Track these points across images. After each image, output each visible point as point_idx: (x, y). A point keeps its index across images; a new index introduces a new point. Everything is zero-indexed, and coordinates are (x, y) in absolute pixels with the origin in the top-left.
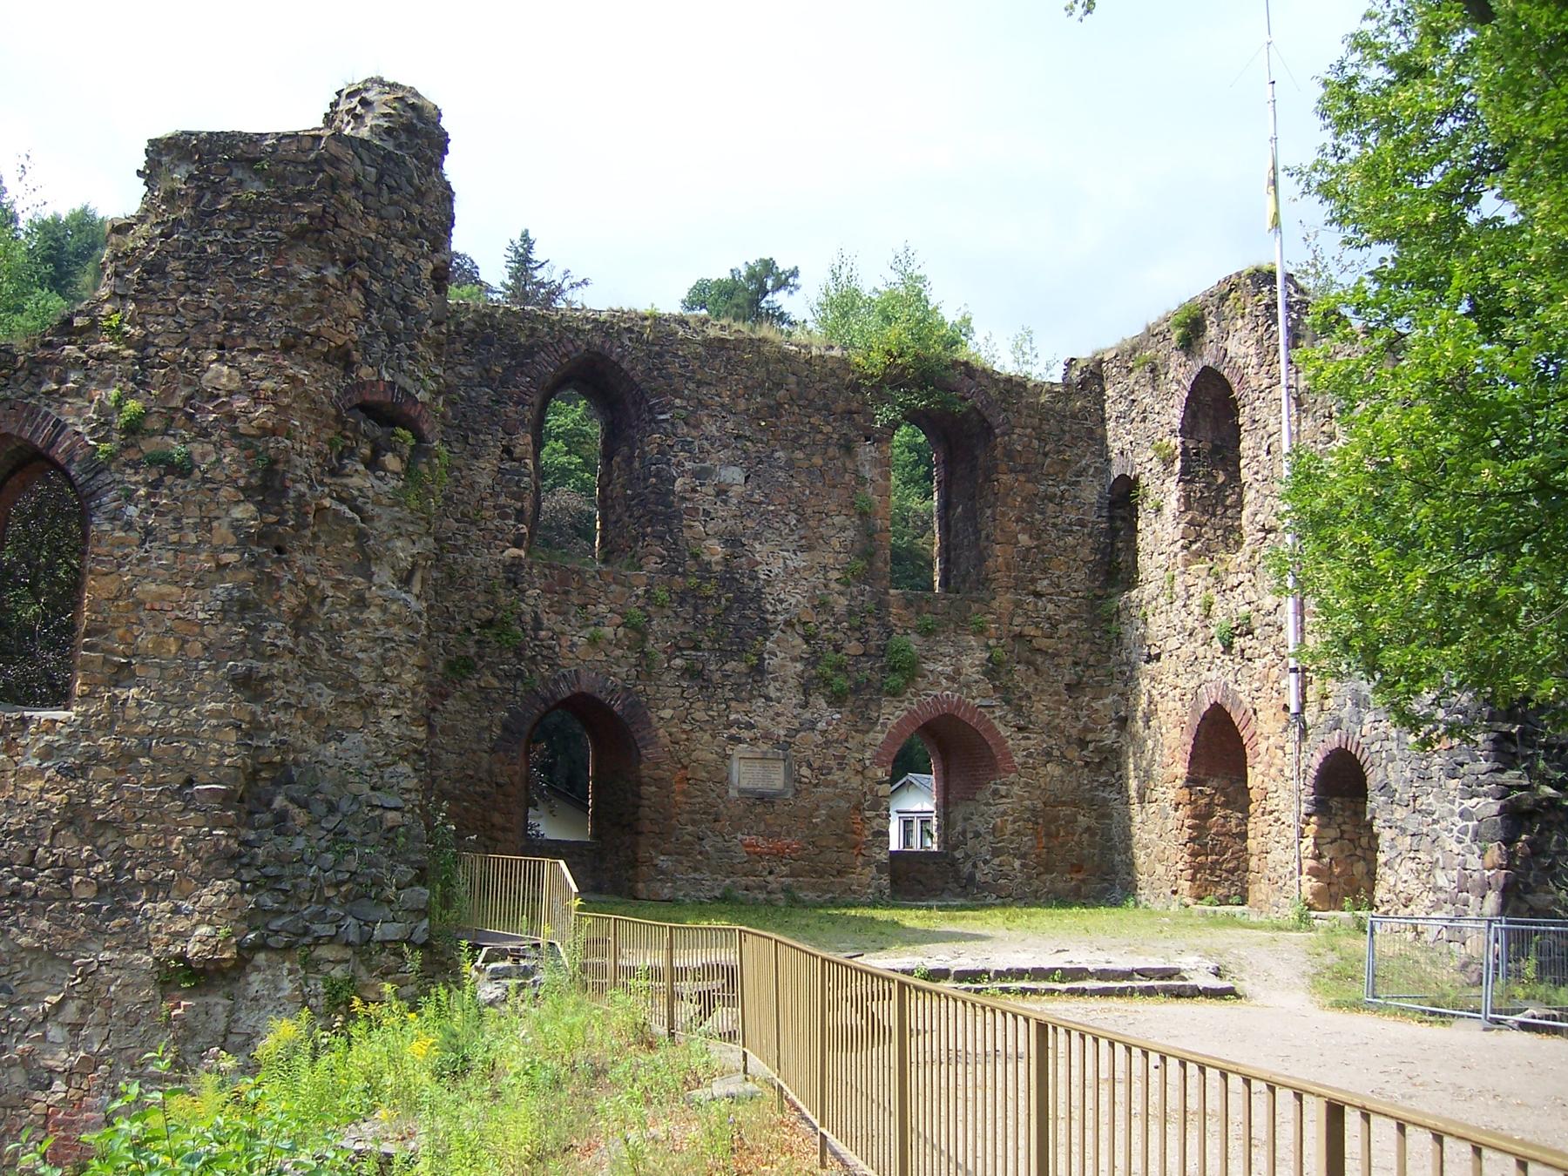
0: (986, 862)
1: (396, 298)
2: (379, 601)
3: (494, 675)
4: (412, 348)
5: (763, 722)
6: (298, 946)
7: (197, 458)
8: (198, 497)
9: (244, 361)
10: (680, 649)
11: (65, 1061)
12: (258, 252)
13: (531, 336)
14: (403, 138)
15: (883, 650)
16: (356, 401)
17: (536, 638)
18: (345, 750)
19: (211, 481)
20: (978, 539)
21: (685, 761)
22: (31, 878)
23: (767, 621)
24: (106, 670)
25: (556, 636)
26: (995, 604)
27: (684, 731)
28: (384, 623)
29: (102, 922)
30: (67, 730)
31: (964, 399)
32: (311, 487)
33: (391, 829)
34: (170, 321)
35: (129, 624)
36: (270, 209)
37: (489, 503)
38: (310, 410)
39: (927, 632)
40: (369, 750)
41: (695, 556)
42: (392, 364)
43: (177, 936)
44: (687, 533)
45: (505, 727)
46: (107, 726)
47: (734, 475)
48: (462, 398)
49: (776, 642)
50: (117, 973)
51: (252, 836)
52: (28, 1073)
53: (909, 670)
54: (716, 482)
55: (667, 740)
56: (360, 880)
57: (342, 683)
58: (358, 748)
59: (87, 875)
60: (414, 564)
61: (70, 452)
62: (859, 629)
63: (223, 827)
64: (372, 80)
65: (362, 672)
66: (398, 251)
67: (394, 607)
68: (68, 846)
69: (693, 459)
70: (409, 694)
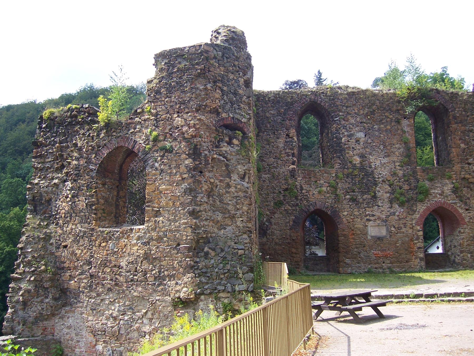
0: (458, 255)
1: (232, 91)
2: (234, 185)
3: (289, 205)
4: (239, 106)
5: (377, 214)
6: (214, 293)
7: (174, 147)
8: (175, 159)
9: (185, 116)
10: (348, 192)
11: (148, 329)
12: (186, 82)
13: (292, 98)
14: (231, 42)
15: (416, 187)
16: (221, 124)
17: (302, 193)
18: (226, 232)
19: (178, 153)
20: (447, 147)
21: (353, 228)
22: (136, 276)
23: (376, 181)
24: (153, 213)
25: (308, 191)
26: (454, 168)
27: (351, 219)
28: (236, 191)
29: (156, 288)
30: (143, 231)
31: (437, 101)
32: (209, 152)
33: (240, 256)
34: (163, 107)
35: (158, 198)
36: (189, 69)
37: (283, 152)
38: (207, 128)
39: (431, 180)
40: (236, 231)
41: (351, 162)
42: (232, 111)
43: (177, 291)
44: (347, 155)
45: (294, 221)
46: (154, 230)
47: (361, 135)
48: (272, 121)
49: (380, 188)
50: (161, 303)
51: (198, 260)
52: (139, 333)
53: (426, 193)
54: (355, 137)
55: (346, 222)
56: (231, 272)
57: (224, 211)
58: (231, 231)
59: (151, 274)
60: (245, 173)
61: (139, 150)
62: (408, 181)
63: (189, 258)
64: (221, 26)
65: (230, 207)
66: (231, 76)
67: (239, 187)
68: (146, 266)
69: (347, 131)
70: (246, 213)
